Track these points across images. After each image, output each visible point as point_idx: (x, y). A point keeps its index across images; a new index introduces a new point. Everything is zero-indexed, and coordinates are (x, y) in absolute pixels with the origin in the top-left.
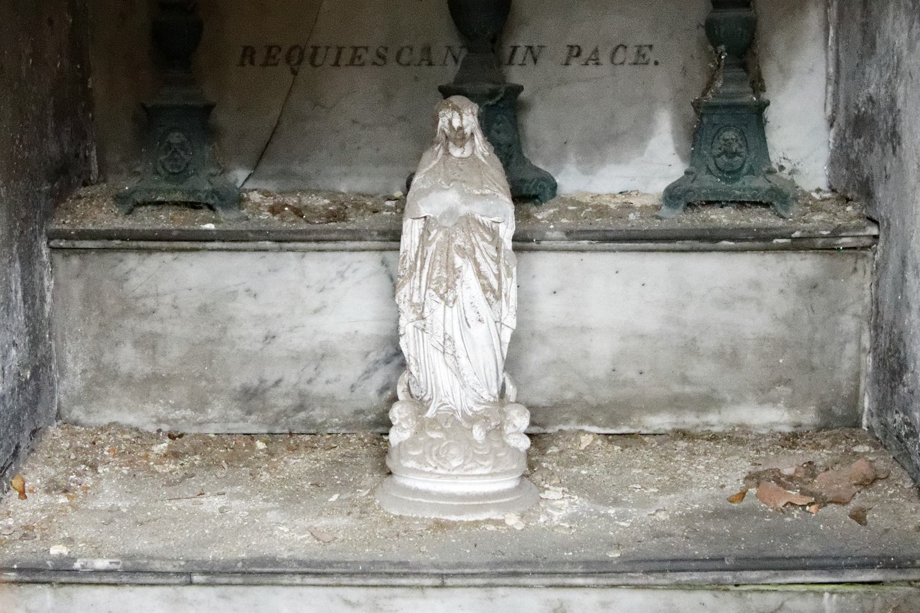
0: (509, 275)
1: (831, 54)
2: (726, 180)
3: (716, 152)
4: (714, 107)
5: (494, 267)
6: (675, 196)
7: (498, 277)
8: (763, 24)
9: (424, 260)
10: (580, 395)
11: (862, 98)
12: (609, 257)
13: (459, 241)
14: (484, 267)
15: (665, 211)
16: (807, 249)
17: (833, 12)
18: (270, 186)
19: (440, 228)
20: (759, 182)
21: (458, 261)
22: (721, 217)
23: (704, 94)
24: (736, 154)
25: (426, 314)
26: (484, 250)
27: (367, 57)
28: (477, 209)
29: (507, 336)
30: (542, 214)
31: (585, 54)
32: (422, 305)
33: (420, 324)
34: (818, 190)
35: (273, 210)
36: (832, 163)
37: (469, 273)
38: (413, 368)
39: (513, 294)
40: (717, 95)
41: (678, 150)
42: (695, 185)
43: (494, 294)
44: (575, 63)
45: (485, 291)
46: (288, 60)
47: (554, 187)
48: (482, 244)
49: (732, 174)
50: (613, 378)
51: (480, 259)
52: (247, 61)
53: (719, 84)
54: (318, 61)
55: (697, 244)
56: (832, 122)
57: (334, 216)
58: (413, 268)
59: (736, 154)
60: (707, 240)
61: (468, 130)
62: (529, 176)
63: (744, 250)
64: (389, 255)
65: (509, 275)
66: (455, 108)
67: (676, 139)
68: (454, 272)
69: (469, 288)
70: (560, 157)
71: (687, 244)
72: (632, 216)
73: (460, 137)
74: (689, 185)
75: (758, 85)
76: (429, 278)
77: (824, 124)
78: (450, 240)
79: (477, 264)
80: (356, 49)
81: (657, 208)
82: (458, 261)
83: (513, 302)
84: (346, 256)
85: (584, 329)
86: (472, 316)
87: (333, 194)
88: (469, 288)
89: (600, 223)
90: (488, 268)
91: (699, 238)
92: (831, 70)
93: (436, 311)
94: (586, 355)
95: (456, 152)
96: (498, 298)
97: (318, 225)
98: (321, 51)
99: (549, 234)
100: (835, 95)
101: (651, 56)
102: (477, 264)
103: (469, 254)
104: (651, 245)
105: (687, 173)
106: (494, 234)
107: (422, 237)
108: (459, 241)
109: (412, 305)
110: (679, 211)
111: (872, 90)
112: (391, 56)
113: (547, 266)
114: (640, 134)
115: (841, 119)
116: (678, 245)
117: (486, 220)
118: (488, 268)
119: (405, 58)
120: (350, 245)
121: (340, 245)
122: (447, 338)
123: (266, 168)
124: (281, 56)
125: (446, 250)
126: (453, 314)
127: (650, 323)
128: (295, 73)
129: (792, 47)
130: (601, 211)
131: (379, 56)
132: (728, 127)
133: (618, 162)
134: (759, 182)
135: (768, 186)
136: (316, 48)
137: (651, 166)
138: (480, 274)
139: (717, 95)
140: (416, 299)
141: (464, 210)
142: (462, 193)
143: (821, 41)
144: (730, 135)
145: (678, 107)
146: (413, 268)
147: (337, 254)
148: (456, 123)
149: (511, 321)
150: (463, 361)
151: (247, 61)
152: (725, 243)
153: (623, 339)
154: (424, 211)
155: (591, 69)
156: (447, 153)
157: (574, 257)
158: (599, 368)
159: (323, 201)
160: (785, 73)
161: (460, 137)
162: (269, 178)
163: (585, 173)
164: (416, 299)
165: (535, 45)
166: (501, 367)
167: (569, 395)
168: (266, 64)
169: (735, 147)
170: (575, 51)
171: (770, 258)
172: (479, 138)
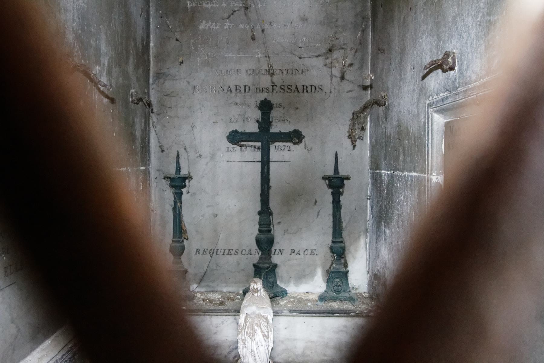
0: (271, 331)
1: (368, 252)
2: (337, 294)
3: (334, 285)
4: (333, 272)
5: (266, 329)
6: (322, 298)
7: (268, 332)
8: (347, 244)
9: (246, 327)
10: (294, 359)
11: (376, 270)
12: (302, 318)
13: (256, 322)
14: (263, 329)
15: (319, 303)
16: (360, 316)
17: (368, 240)
18: (203, 290)
19: (251, 317)
20: (346, 294)
21: (256, 328)
22: (335, 305)
23: (330, 268)
24: (340, 286)
25: (246, 343)
26: (263, 324)
27: (233, 252)
28: (262, 312)
29: (270, 349)
30: (283, 302)
31: (296, 252)
32: (245, 340)
33: (244, 346)
34: (364, 293)
35: (204, 300)
36: (369, 285)
37: (259, 331)
38: (242, 359)
39: (272, 337)
40: (334, 268)
41: (323, 280)
42: (328, 295)
43: (266, 337)
44: (293, 254)
45: (263, 336)
46: (210, 253)
47: (287, 293)
48: (263, 322)
49: (338, 292)
50: (303, 354)
51: (262, 327)
52: (198, 253)
53: (334, 265)
54: (218, 253)
55: (328, 315)
56: (368, 273)
57: (222, 303)
58: (242, 329)
59: (340, 286)
60: (331, 313)
61: (259, 289)
62: (279, 290)
63: (342, 316)
64: (237, 317)
65: (271, 331)
66: (256, 283)
67: (323, 276)
68: (255, 331)
69: (259, 336)
70: (288, 282)
71: (325, 314)
72: (309, 304)
73: (256, 291)
74: (325, 295)
75: (346, 265)
76: (247, 333)
77: (366, 273)
78: (253, 321)
79: (261, 328)
80: (229, 250)
81: (317, 301)
82: (256, 328)
83: (272, 339)
84: (224, 317)
85: (295, 340)
86: (260, 344)
87: (221, 292)
88: (259, 336)
89: (301, 307)
90: (265, 330)
91: (329, 313)
92: (368, 257)
93: (249, 341)
94: (295, 348)
95: (256, 295)
96: (267, 338)
97: (216, 307)
98: (219, 251)
99: (284, 311)
100: (369, 264)
101: (315, 252)
102: (261, 328)
103: (259, 325)
104: (314, 315)
105: (325, 291)
106: (266, 318)
107: (245, 319)
108: (256, 322)
109: (242, 340)
110: (323, 303)
111: (379, 268)
112: (239, 252)
113: (283, 321)
114: (312, 275)
115: (370, 272)
116: (322, 315)
117: (264, 315)
118: (265, 330)
119: (244, 252)
120: (225, 314)
121: (222, 314)
122: (252, 351)
123: (203, 284)
124: (208, 252)
125: (252, 324)
126: (254, 343)
127: (314, 338)
128: (211, 257)
129: (356, 250)
130: (300, 301)
131: (281, 88)
132: (337, 278)
133: (306, 283)
134: (346, 294)
135: (349, 296)
136: (218, 250)
137: (316, 285)
138: (262, 332)
139: (334, 268)
140: (243, 338)
141: (257, 312)
142: (257, 307)
143: (365, 248)
144: (337, 280)
145: (323, 268)
146: (242, 329)
147: (221, 317)
148: (255, 287)
149: (271, 345)
150: (257, 357)
151: (198, 253)
152: (336, 314)
153: (306, 342)
154: (246, 312)
155: (298, 256)
156: (253, 295)
157: (292, 318)
158: (299, 351)
159: (218, 296)
160: (354, 258)
161: (256, 291)
162: (203, 287)
163: (296, 286)
164: (243, 338)
165: (281, 249)
166: (268, 358)
167: (290, 359)
168: (203, 254)
169: (339, 284)
170: (293, 251)
171: (350, 319)
172: (262, 290)
